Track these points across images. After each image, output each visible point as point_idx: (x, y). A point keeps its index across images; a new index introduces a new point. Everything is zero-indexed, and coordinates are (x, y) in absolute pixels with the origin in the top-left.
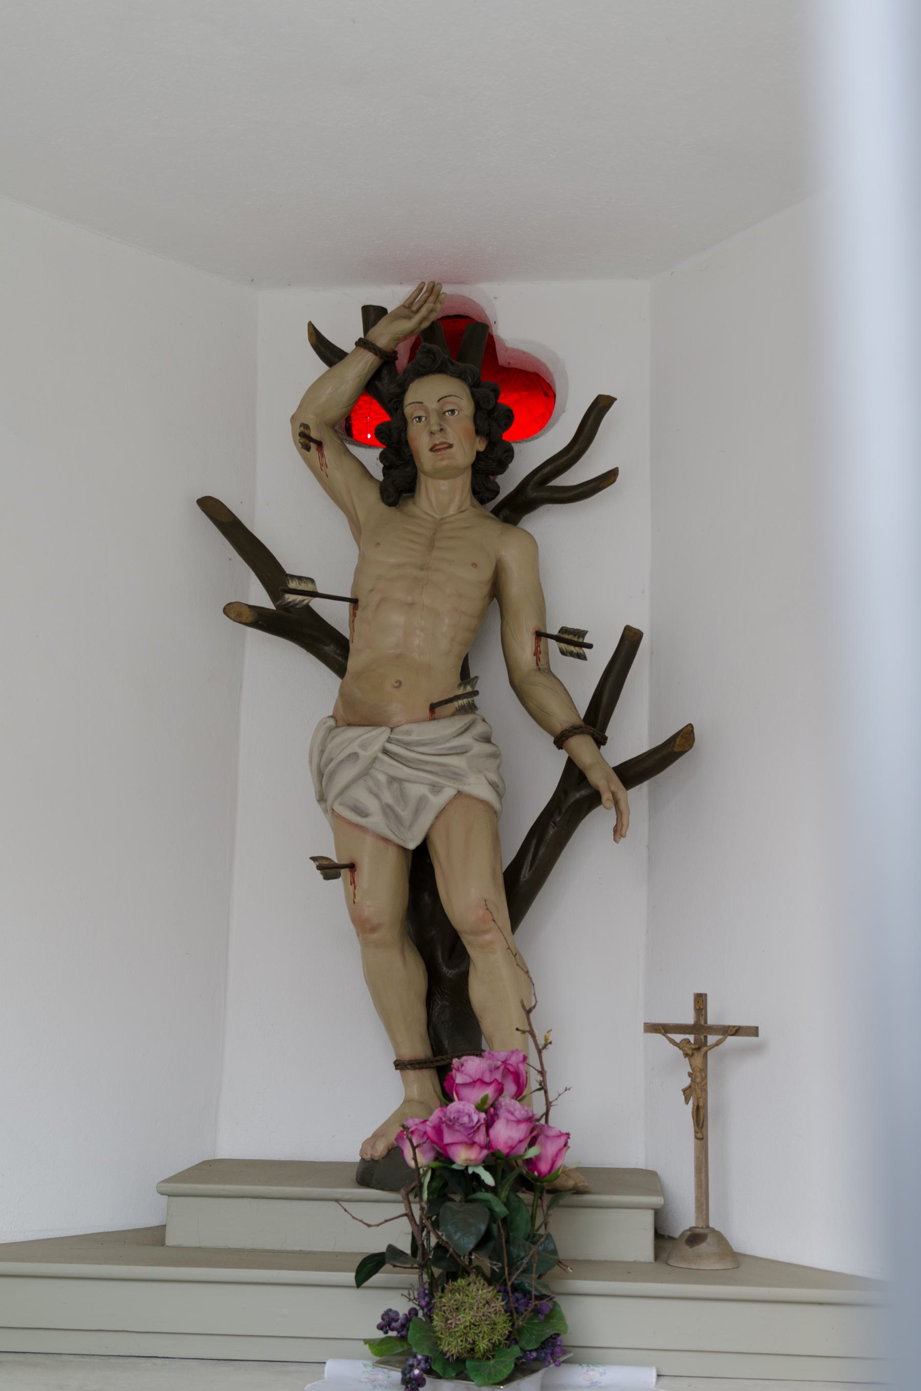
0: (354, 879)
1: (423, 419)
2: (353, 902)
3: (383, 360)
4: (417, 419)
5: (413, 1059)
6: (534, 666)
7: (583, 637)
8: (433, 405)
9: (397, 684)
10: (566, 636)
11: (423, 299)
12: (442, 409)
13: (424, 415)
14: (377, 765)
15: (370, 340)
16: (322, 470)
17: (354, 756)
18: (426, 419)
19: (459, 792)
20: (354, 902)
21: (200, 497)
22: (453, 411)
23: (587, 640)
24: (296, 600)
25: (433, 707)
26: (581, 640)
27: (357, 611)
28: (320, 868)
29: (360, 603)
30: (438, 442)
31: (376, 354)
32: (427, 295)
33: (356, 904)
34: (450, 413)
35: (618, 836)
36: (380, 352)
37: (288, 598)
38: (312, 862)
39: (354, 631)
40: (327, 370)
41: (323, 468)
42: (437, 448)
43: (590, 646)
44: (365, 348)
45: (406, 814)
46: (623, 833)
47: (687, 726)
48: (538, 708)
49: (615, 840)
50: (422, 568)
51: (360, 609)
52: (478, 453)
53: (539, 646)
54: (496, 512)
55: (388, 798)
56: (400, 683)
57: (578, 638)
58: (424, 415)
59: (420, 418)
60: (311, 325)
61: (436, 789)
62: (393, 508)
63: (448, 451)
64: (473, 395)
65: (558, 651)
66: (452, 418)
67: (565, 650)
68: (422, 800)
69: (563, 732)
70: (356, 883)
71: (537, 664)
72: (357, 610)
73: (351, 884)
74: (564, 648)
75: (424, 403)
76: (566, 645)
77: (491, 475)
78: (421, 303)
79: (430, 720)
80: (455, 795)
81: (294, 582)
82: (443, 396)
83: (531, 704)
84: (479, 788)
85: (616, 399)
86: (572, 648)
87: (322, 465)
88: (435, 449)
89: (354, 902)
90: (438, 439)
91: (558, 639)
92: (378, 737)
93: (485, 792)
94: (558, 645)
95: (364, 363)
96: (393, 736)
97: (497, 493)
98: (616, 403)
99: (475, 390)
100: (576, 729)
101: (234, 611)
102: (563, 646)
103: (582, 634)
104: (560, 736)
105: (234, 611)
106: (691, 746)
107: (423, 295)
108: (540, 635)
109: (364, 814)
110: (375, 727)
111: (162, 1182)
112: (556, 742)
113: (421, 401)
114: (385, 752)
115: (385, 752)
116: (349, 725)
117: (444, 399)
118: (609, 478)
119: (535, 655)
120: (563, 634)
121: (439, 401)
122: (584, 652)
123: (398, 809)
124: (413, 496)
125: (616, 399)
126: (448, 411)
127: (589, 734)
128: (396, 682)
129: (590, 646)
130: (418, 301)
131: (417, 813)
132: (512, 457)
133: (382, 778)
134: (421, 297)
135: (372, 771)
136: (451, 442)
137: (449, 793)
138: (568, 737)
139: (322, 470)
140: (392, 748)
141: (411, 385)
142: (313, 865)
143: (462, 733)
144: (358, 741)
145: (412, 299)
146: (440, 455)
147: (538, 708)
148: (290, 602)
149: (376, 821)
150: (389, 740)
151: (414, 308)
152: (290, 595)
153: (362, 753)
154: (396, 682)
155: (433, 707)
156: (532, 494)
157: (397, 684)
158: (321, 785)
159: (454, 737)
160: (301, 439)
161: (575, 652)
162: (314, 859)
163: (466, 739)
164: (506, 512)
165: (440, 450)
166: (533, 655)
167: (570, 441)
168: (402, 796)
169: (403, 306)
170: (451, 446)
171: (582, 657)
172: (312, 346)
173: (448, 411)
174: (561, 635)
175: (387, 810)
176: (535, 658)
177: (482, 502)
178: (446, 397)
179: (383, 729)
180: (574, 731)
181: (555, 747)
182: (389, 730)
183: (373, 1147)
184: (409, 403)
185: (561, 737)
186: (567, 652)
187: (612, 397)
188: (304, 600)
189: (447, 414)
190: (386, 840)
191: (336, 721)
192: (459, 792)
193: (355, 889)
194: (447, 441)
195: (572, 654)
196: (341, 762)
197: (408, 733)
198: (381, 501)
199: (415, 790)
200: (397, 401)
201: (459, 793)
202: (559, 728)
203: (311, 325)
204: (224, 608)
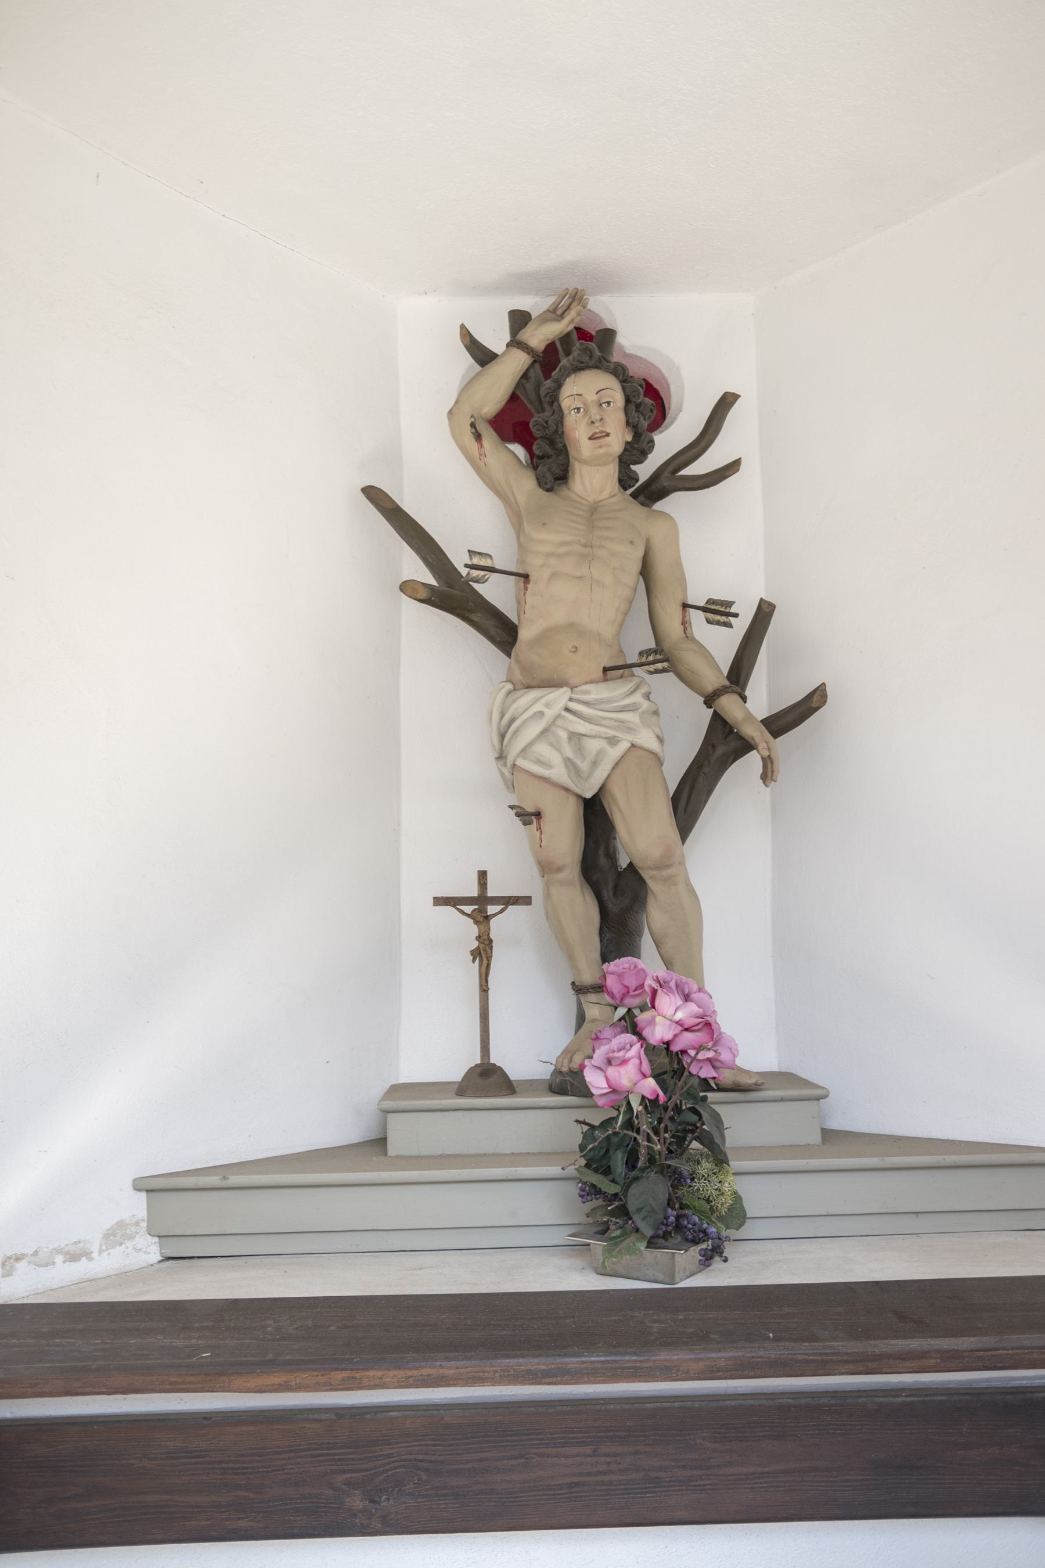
0: (540, 825)
1: (582, 410)
2: (539, 845)
3: (533, 359)
4: (576, 410)
5: (593, 983)
6: (684, 635)
7: (730, 607)
8: (591, 397)
9: (574, 650)
10: (713, 607)
11: (566, 304)
12: (599, 401)
13: (582, 406)
14: (559, 722)
15: (523, 341)
16: (480, 459)
17: (541, 714)
18: (584, 410)
19: (632, 744)
20: (541, 846)
21: (363, 486)
22: (609, 403)
23: (733, 610)
24: (479, 575)
25: (605, 670)
26: (728, 610)
27: (528, 585)
28: (518, 815)
29: (531, 578)
30: (597, 431)
31: (528, 353)
32: (570, 301)
33: (542, 848)
34: (606, 404)
35: (768, 781)
36: (532, 351)
37: (473, 574)
38: (510, 809)
39: (526, 604)
40: (479, 370)
41: (482, 458)
42: (596, 436)
43: (736, 615)
44: (518, 348)
45: (584, 766)
46: (774, 778)
47: (821, 685)
48: (690, 671)
49: (766, 785)
50: (586, 546)
51: (531, 583)
52: (627, 443)
53: (686, 617)
54: (634, 496)
55: (569, 753)
56: (576, 648)
57: (726, 608)
58: (582, 406)
59: (578, 409)
60: (462, 327)
61: (613, 741)
62: (550, 493)
63: (606, 438)
64: (624, 389)
65: (705, 620)
66: (609, 409)
67: (711, 620)
68: (600, 753)
69: (715, 691)
70: (542, 828)
71: (685, 633)
72: (529, 584)
73: (537, 830)
74: (710, 618)
75: (584, 396)
76: (712, 615)
77: (633, 464)
78: (564, 308)
79: (604, 681)
80: (630, 748)
81: (476, 558)
82: (601, 389)
83: (682, 667)
84: (647, 739)
85: (739, 396)
86: (718, 617)
87: (481, 455)
88: (594, 437)
89: (541, 846)
90: (597, 428)
91: (704, 609)
92: (559, 697)
93: (653, 744)
94: (704, 615)
95: (517, 363)
96: (574, 696)
97: (637, 480)
98: (740, 399)
99: (624, 384)
100: (727, 688)
101: (407, 588)
102: (710, 616)
103: (730, 604)
104: (712, 695)
105: (407, 588)
106: (825, 702)
107: (566, 300)
108: (685, 606)
109: (548, 765)
110: (556, 688)
111: (576, 1033)
112: (705, 703)
113: (581, 394)
114: (567, 710)
115: (567, 710)
116: (529, 687)
117: (601, 392)
118: (733, 467)
119: (682, 625)
120: (710, 604)
121: (597, 393)
122: (730, 621)
123: (578, 762)
124: (566, 483)
125: (739, 396)
126: (605, 403)
127: (737, 693)
128: (573, 648)
129: (736, 615)
130: (563, 305)
131: (595, 764)
132: (653, 447)
133: (564, 735)
134: (565, 302)
135: (553, 728)
136: (608, 431)
137: (624, 746)
138: (719, 696)
139: (480, 459)
140: (573, 706)
141: (568, 379)
142: (512, 813)
143: (633, 692)
144: (543, 700)
145: (556, 305)
146: (599, 443)
147: (690, 671)
148: (474, 577)
149: (559, 773)
150: (571, 700)
151: (559, 312)
152: (474, 571)
153: (545, 710)
154: (573, 648)
155: (605, 670)
156: (664, 481)
157: (574, 650)
158: (502, 745)
159: (627, 695)
160: (471, 429)
161: (722, 620)
162: (512, 807)
163: (637, 698)
164: (642, 498)
165: (599, 438)
166: (680, 625)
167: (698, 434)
168: (580, 750)
169: (548, 310)
170: (608, 435)
171: (728, 625)
172: (466, 347)
173: (605, 403)
174: (709, 606)
175: (568, 762)
176: (683, 626)
177: (625, 489)
178: (603, 390)
179: (565, 689)
180: (725, 690)
181: (705, 706)
182: (569, 690)
183: (570, 1061)
184: (569, 395)
185: (713, 696)
186: (713, 621)
187: (737, 394)
188: (485, 575)
189: (604, 405)
190: (567, 790)
191: (514, 684)
192: (632, 744)
193: (541, 834)
194: (604, 429)
195: (718, 623)
196: (525, 721)
197: (587, 692)
198: (538, 488)
199: (593, 746)
200: (552, 395)
201: (633, 746)
202: (710, 688)
203: (462, 327)
204: (401, 586)
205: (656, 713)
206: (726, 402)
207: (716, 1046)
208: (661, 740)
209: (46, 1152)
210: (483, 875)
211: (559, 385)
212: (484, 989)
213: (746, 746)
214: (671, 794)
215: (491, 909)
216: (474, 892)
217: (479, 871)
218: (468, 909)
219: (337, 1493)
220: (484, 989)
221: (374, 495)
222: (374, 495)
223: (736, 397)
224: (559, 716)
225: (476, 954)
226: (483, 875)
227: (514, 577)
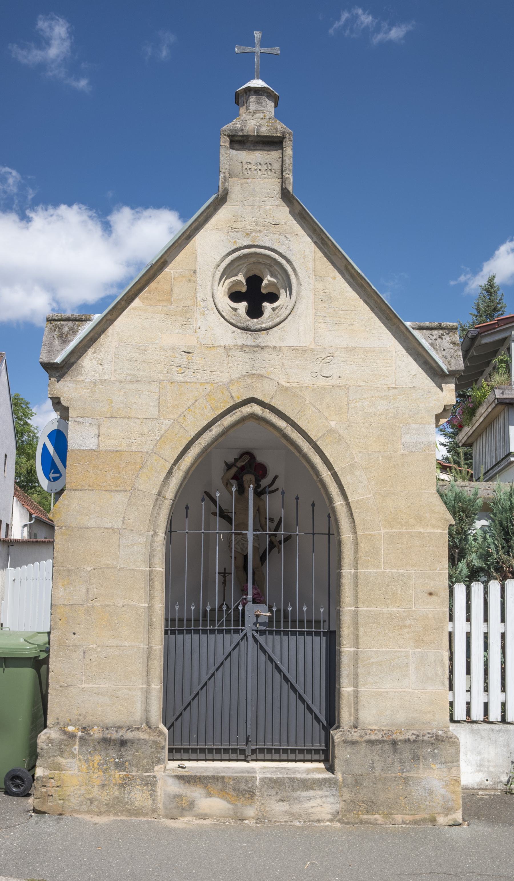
103: (273, 519)
133: (241, 543)
140: (242, 538)
175: (241, 549)
205: (258, 539)
206: (276, 477)
207: (60, 739)
208: (259, 545)
209: (431, 594)
210: (225, 569)
211: (243, 476)
212: (224, 589)
213: (275, 546)
214: (261, 555)
215: (226, 575)
216: (223, 572)
217: (450, 722)
218: (222, 575)
219: (96, 765)
220: (224, 589)
221: (206, 493)
222: (206, 493)
223: (278, 476)
224: (239, 540)
225: (223, 583)
226: (225, 569)
227: (136, 303)
